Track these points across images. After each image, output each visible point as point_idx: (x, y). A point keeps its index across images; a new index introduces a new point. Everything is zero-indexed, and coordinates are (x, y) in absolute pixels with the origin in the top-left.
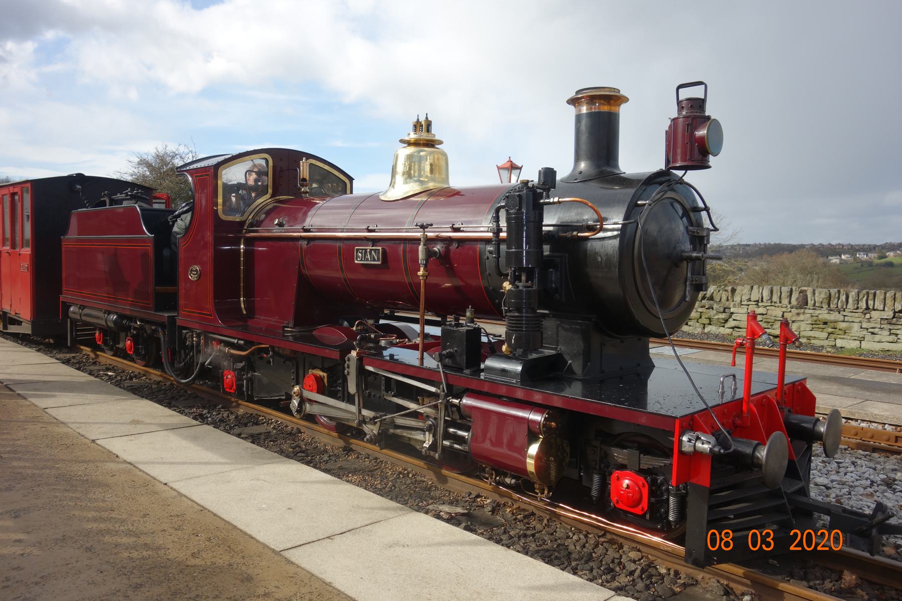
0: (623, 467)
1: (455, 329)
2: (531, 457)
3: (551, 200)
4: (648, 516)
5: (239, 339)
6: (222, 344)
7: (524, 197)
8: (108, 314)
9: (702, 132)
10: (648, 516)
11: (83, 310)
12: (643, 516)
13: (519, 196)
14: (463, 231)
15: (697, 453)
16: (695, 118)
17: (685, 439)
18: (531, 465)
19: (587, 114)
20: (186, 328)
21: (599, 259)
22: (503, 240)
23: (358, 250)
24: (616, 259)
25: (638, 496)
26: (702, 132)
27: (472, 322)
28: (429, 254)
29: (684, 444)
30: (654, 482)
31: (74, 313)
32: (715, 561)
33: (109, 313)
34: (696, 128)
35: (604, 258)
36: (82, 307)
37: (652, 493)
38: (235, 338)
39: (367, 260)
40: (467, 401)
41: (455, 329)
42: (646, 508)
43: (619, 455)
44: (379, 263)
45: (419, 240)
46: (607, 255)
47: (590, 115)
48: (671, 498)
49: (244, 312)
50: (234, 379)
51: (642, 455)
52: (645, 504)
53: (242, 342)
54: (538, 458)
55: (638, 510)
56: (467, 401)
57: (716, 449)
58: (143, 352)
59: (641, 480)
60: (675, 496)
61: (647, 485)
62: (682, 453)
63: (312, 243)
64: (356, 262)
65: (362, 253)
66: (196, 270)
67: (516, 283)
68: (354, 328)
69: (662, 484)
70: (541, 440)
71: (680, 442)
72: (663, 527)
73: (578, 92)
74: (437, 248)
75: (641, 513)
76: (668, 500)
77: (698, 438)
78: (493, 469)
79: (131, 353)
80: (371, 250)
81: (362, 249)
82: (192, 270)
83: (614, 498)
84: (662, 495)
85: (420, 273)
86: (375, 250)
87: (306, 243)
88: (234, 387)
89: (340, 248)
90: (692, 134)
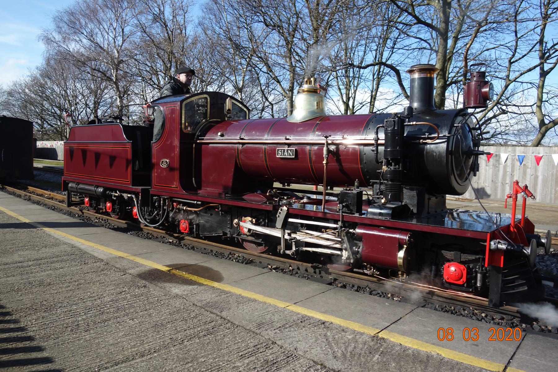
0: (449, 261)
1: (350, 192)
2: (400, 258)
3: (411, 123)
4: (465, 285)
5: (197, 201)
6: (181, 205)
7: (396, 122)
8: (97, 188)
9: (486, 90)
10: (465, 285)
11: (78, 185)
12: (463, 285)
13: (394, 121)
14: (245, 140)
15: (498, 250)
16: (481, 82)
17: (492, 243)
18: (400, 261)
19: (418, 78)
20: (155, 196)
21: (435, 154)
22: (381, 145)
23: (278, 150)
24: (445, 154)
25: (460, 274)
26: (486, 90)
27: (358, 188)
28: (329, 151)
29: (492, 246)
30: (468, 268)
31: (72, 187)
32: (504, 304)
33: (97, 187)
34: (483, 87)
35: (438, 154)
36: (78, 184)
37: (468, 273)
38: (194, 201)
39: (285, 155)
40: (358, 231)
41: (350, 192)
42: (465, 281)
43: (448, 254)
44: (294, 157)
45: (324, 144)
46: (439, 152)
47: (420, 79)
48: (479, 275)
49: (195, 186)
50: (188, 225)
51: (462, 254)
52: (464, 279)
53: (200, 203)
54: (404, 259)
55: (460, 282)
56: (358, 231)
57: (509, 247)
58: (118, 211)
59: (462, 267)
60: (481, 273)
61: (466, 269)
62: (490, 250)
63: (245, 146)
64: (277, 156)
65: (281, 152)
66: (166, 162)
67: (389, 166)
68: (268, 194)
69: (473, 268)
70: (405, 248)
71: (490, 244)
72: (472, 290)
73: (412, 67)
74: (332, 148)
75: (462, 283)
76: (476, 276)
77: (499, 242)
78: (371, 265)
79: (110, 211)
80: (288, 150)
81: (282, 150)
82: (163, 162)
83: (446, 277)
84: (473, 274)
85: (324, 162)
86: (291, 150)
87: (241, 146)
88: (188, 230)
89: (265, 149)
90: (480, 91)
